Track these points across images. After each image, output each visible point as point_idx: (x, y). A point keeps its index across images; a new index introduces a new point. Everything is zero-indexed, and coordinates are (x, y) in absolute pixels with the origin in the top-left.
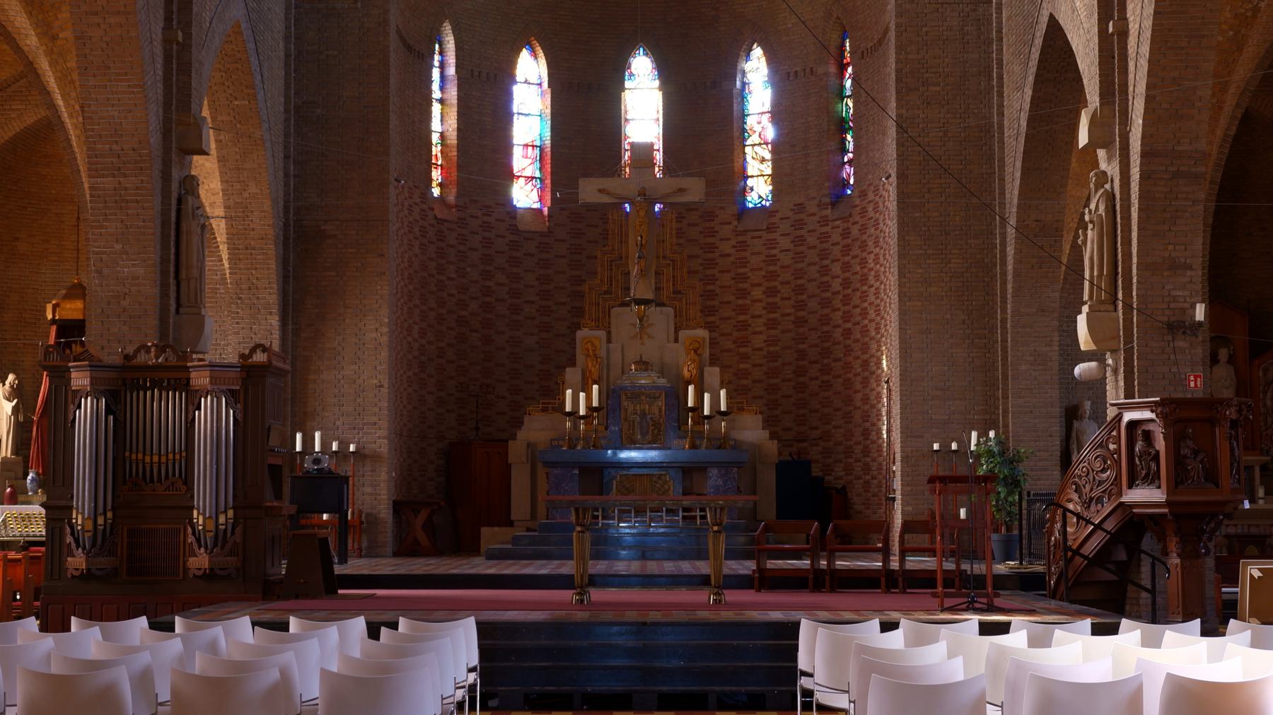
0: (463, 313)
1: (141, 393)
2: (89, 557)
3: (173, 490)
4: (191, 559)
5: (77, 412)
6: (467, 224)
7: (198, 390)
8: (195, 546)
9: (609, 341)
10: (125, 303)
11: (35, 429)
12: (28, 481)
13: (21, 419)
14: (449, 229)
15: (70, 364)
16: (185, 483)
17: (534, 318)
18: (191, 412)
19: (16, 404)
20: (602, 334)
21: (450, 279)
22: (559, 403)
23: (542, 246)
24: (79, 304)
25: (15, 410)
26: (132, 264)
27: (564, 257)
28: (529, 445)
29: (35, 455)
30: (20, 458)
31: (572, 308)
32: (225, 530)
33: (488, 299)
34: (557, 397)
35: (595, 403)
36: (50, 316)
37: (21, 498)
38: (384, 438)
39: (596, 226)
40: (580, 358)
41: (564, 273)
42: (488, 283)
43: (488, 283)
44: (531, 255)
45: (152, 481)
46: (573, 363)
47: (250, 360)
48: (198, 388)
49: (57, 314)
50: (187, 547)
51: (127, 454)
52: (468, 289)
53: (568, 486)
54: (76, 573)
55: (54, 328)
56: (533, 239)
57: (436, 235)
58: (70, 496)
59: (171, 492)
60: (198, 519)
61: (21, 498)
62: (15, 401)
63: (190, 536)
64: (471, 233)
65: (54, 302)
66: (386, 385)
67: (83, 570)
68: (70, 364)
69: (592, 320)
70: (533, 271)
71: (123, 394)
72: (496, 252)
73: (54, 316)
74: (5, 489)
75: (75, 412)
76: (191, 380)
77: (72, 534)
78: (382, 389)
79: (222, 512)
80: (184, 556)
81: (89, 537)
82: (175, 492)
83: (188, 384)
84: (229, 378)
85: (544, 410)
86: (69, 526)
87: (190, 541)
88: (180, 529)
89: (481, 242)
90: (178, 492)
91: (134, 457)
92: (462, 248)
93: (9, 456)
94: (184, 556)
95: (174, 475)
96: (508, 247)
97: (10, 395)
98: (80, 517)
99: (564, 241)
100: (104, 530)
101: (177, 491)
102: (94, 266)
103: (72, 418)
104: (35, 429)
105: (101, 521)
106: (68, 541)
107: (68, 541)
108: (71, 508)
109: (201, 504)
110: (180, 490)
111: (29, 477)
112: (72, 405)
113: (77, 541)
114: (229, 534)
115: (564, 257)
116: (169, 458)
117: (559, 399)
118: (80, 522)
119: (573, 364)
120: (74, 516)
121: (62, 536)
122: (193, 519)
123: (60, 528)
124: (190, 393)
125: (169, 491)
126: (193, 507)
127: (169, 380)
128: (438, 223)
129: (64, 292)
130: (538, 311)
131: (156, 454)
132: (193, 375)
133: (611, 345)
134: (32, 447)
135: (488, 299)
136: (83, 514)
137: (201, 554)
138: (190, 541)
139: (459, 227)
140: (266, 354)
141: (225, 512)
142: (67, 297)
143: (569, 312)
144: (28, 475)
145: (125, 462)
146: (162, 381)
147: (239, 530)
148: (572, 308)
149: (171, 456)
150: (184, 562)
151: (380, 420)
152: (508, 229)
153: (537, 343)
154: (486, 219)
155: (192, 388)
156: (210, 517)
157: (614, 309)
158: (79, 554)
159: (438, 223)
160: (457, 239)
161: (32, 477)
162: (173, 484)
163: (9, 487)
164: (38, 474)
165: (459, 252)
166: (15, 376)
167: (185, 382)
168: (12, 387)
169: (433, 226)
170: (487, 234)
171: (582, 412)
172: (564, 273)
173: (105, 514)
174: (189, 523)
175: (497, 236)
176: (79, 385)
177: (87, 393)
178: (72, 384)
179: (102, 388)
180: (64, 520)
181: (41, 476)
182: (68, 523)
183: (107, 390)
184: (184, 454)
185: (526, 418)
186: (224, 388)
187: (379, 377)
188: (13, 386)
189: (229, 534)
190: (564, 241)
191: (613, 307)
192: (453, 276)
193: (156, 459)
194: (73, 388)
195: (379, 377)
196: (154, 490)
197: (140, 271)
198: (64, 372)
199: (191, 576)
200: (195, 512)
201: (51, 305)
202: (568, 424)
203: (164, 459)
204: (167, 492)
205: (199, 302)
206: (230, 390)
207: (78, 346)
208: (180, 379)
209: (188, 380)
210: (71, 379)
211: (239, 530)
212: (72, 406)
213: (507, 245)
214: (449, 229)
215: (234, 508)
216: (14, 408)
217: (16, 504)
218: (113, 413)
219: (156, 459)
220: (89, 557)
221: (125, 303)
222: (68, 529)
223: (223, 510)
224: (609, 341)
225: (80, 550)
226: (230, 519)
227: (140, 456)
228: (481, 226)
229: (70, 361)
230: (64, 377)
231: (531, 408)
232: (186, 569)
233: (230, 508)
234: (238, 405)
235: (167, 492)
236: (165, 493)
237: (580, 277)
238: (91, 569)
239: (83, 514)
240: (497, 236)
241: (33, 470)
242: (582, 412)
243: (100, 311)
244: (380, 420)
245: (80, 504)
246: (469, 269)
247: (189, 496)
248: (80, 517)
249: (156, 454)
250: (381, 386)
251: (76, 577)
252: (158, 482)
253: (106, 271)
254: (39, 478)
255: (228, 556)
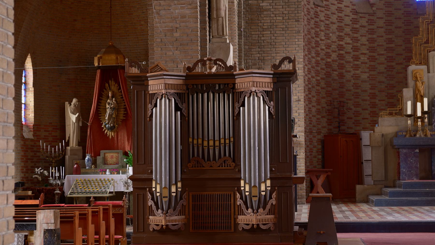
0: (329, 60)
1: (200, 95)
2: (167, 216)
3: (225, 166)
4: (240, 217)
5: (154, 110)
6: (330, 8)
7: (242, 92)
8: (243, 207)
9: (429, 72)
10: (177, 35)
11: (89, 130)
12: (86, 161)
13: (81, 124)
14: (321, 11)
15: (148, 75)
16: (234, 161)
17: (366, 63)
18: (237, 108)
19: (77, 116)
20: (424, 67)
21: (321, 40)
22: (399, 110)
23: (369, 21)
24: (113, 57)
25: (78, 119)
26: (181, 7)
27: (382, 27)
28: (383, 135)
29: (89, 145)
30: (81, 148)
31: (387, 57)
32: (265, 196)
33: (341, 52)
34: (398, 106)
35: (426, 109)
36: (96, 64)
37: (82, 170)
38: (301, 132)
39: (400, 9)
40: (411, 82)
41: (382, 36)
42: (341, 43)
43: (341, 43)
44: (364, 27)
45: (209, 159)
46: (406, 86)
47: (280, 69)
48: (242, 90)
49: (100, 63)
50: (236, 209)
51: (191, 140)
52: (331, 46)
53: (412, 160)
54: (156, 228)
55: (99, 71)
56: (365, 17)
57: (314, 14)
58: (150, 171)
59: (223, 168)
60: (245, 187)
61: (82, 170)
62: (77, 114)
63: (238, 199)
64: (332, 13)
65: (98, 56)
66: (302, 100)
67: (162, 225)
68: (148, 75)
69: (417, 60)
70: (365, 36)
71: (186, 95)
72: (345, 25)
73: (99, 64)
74: (73, 166)
75: (152, 110)
76: (236, 85)
77: (153, 199)
78: (300, 102)
79: (263, 182)
80: (235, 214)
81: (166, 202)
82: (226, 168)
83: (234, 88)
84: (265, 82)
85: (391, 114)
86: (150, 193)
87: (238, 203)
88: (230, 195)
89: (337, 19)
90: (229, 168)
91: (195, 142)
92: (327, 22)
93: (74, 146)
94: (235, 214)
95: (225, 155)
96: (351, 22)
97: (74, 111)
98: (158, 187)
99: (382, 18)
100: (176, 196)
101: (227, 166)
102: (155, 9)
103: (150, 114)
104: (89, 130)
105: (173, 189)
106: (149, 204)
107: (149, 204)
108: (151, 180)
109: (247, 176)
110: (230, 166)
111: (87, 158)
112: (150, 104)
113: (156, 204)
114: (268, 199)
115: (382, 27)
116: (221, 143)
117: (399, 107)
118: (158, 190)
119: (406, 86)
120: (154, 185)
121: (145, 200)
122: (240, 187)
123: (143, 194)
124: (235, 93)
125: (222, 166)
126: (240, 179)
127: (219, 85)
128: (315, 7)
129: (104, 50)
130: (368, 59)
131: (211, 140)
132: (238, 81)
133: (430, 74)
134: (88, 141)
135: (341, 52)
136: (161, 184)
137: (249, 214)
138: (238, 203)
139: (325, 10)
140: (291, 64)
141: (265, 182)
142: (106, 53)
143: (385, 59)
144: (85, 157)
145: (189, 145)
146: (214, 85)
147: (274, 195)
148: (387, 57)
149: (222, 141)
150: (235, 219)
151: (299, 121)
152: (351, 12)
153: (368, 77)
154: (340, 5)
155: (237, 91)
156: (255, 186)
157: (431, 52)
158: (159, 214)
159: (315, 7)
160: (325, 17)
161: (88, 159)
162: (225, 161)
163: (76, 164)
164: (91, 157)
165: (326, 24)
166: (77, 100)
167: (232, 87)
168: (75, 106)
169: (313, 9)
170: (340, 15)
171: (419, 114)
172: (382, 36)
173: (176, 184)
174: (237, 190)
175: (345, 15)
176: (155, 90)
177: (162, 96)
178: (149, 89)
179: (173, 91)
180: (145, 189)
181: (93, 158)
182: (149, 191)
183: (175, 93)
184: (232, 139)
185: (380, 119)
186: (261, 89)
187: (298, 94)
188: (76, 105)
189: (268, 199)
190: (382, 18)
191: (430, 52)
192: (323, 38)
193: (211, 143)
194: (150, 92)
195: (298, 94)
196: (211, 167)
197: (187, 12)
198: (143, 81)
199: (241, 229)
200: (242, 183)
201: (97, 57)
202: (409, 122)
203: (217, 143)
204: (221, 168)
205: (225, 34)
206: (266, 91)
207: (113, 81)
208: (228, 84)
209: (234, 84)
210: (149, 85)
211: (274, 195)
212: (150, 106)
213: (351, 21)
214: (321, 11)
215: (271, 179)
216: (77, 118)
217: (80, 174)
218: (180, 110)
219: (211, 143)
220: (167, 216)
221: (177, 35)
222: (150, 195)
223: (263, 180)
224: (429, 72)
225: (160, 211)
226: (268, 187)
227: (200, 141)
228: (337, 10)
229: (148, 72)
230: (144, 84)
231: (382, 113)
232: (236, 225)
233: (268, 179)
234: (272, 102)
235: (221, 168)
236: (219, 168)
237: (392, 39)
238: (168, 225)
239: (161, 184)
240: (345, 15)
241: (88, 154)
242: (419, 114)
243: (160, 40)
244: (299, 121)
245: (158, 177)
246: (331, 35)
247: (237, 170)
248: (158, 187)
249: (211, 140)
250: (299, 100)
251: (156, 230)
252: (208, 160)
253: (162, 12)
254: (92, 159)
255: (268, 215)
